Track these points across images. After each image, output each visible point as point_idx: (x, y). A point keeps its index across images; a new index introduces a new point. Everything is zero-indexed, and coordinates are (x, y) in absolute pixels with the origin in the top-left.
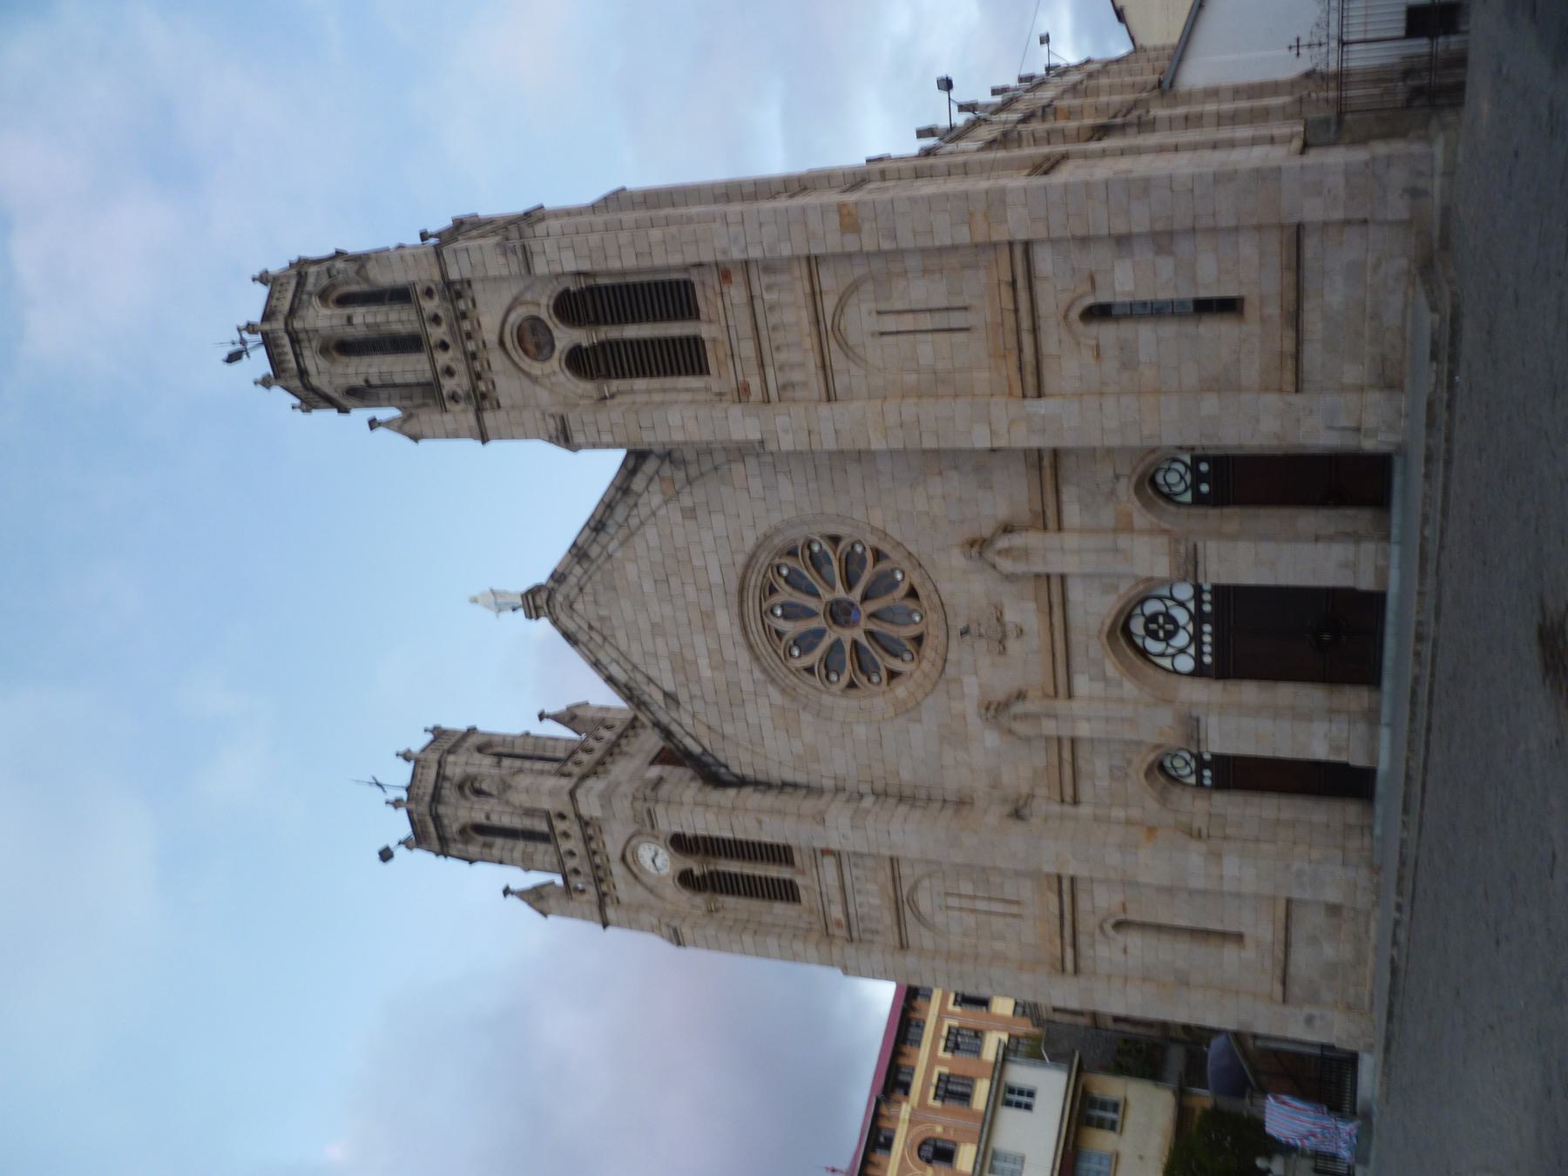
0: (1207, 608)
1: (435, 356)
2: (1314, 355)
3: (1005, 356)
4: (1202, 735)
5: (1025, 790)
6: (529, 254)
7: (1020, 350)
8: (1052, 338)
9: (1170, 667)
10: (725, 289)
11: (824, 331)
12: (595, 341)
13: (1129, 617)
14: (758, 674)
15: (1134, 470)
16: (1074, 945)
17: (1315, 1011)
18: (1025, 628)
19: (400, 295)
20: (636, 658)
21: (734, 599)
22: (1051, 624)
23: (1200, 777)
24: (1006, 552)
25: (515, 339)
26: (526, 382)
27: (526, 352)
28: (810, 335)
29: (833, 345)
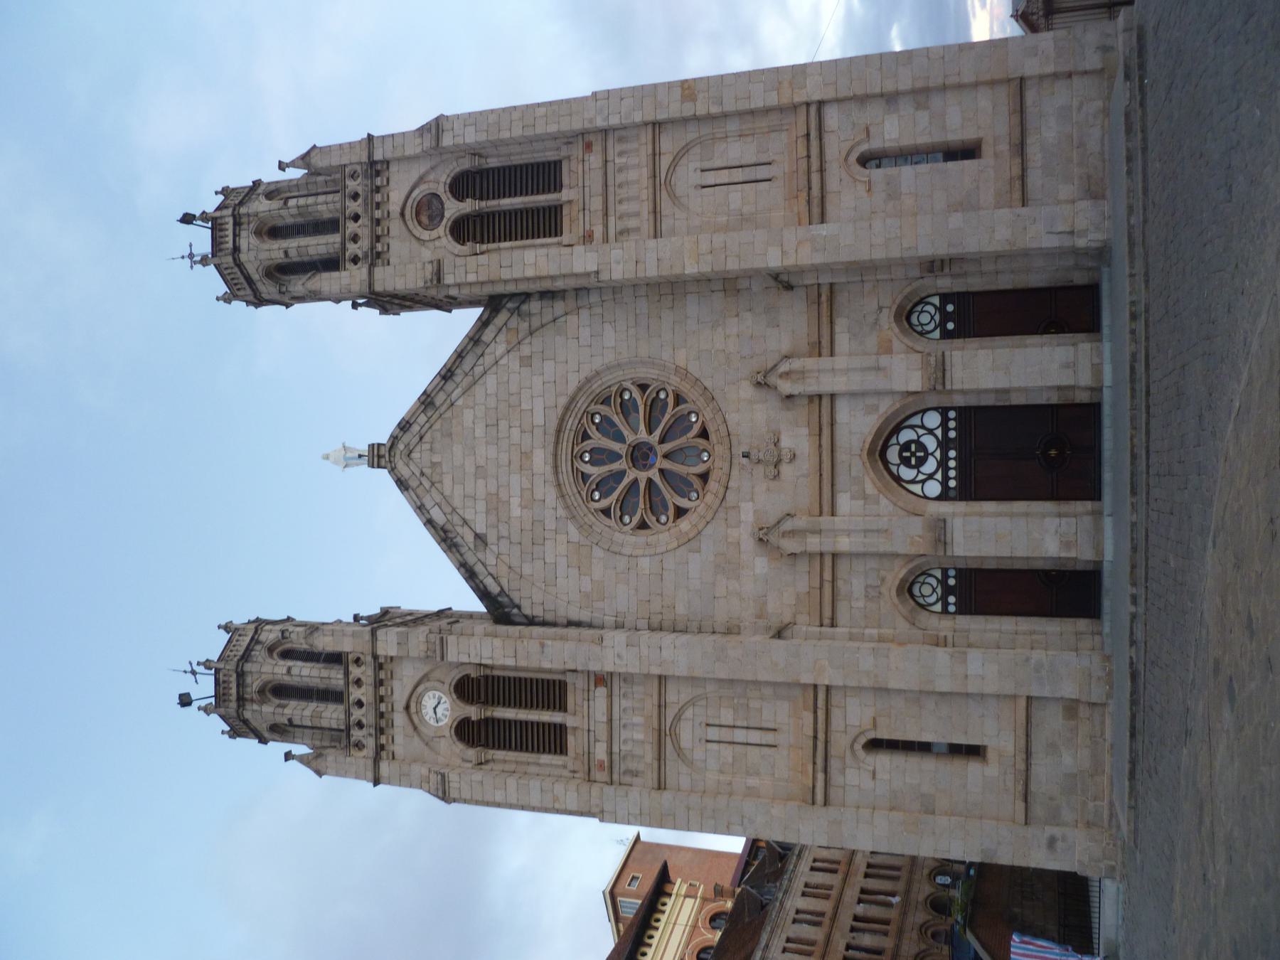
0: (952, 434)
1: (347, 224)
2: (1035, 178)
3: (797, 197)
4: (949, 540)
5: (787, 619)
6: (440, 131)
7: (810, 188)
10: (586, 158)
11: (658, 183)
12: (477, 164)
14: (561, 512)
15: (894, 302)
16: (826, 771)
17: (1056, 831)
18: (798, 453)
19: (335, 659)
20: (457, 502)
21: (552, 439)
22: (820, 446)
24: (786, 375)
25: (414, 210)
26: (415, 243)
27: (420, 223)
28: (647, 188)
29: (664, 193)
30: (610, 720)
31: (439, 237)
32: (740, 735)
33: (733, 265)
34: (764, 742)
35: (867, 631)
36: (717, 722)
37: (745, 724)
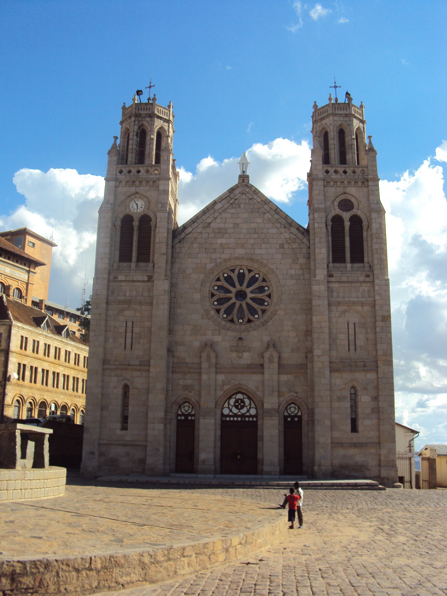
0: (247, 419)
8: (347, 376)
9: (225, 406)
13: (243, 393)
14: (219, 260)
17: (97, 455)
20: (224, 215)
23: (181, 415)
26: (333, 199)
30: (134, 281)
31: (335, 209)
32: (129, 335)
33: (315, 336)
34: (127, 345)
35: (170, 386)
36: (134, 326)
37: (134, 337)
